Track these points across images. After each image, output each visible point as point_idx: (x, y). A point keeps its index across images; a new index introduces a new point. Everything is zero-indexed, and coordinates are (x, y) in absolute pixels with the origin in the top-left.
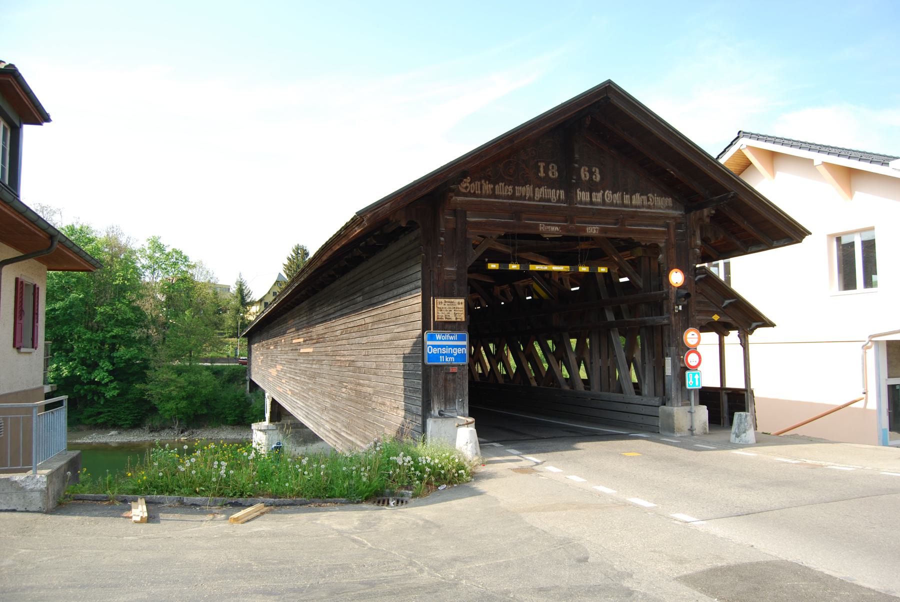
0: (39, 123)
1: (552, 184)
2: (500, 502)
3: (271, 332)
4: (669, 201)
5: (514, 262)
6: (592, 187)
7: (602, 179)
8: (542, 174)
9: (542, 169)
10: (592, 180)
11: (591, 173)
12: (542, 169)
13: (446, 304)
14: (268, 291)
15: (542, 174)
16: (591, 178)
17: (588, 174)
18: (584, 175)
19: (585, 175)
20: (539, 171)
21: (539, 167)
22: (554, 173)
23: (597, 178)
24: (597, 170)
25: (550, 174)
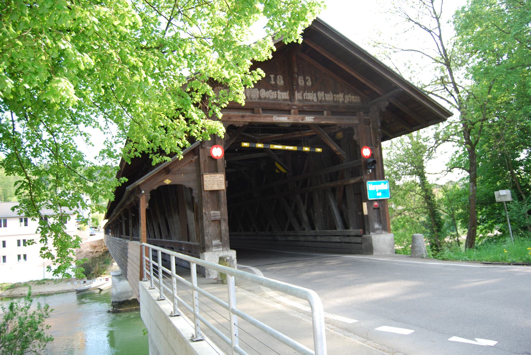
0: (451, 116)
1: (284, 89)
2: (92, 219)
3: (269, 268)
4: (225, 131)
5: (260, 143)
6: (306, 89)
7: (312, 84)
8: (273, 82)
9: (272, 79)
10: (307, 85)
11: (306, 81)
12: (272, 79)
13: (211, 178)
14: (14, 282)
15: (273, 82)
16: (305, 83)
17: (303, 81)
18: (301, 82)
19: (301, 82)
20: (271, 81)
21: (270, 77)
22: (281, 82)
23: (309, 83)
24: (310, 79)
25: (278, 83)
